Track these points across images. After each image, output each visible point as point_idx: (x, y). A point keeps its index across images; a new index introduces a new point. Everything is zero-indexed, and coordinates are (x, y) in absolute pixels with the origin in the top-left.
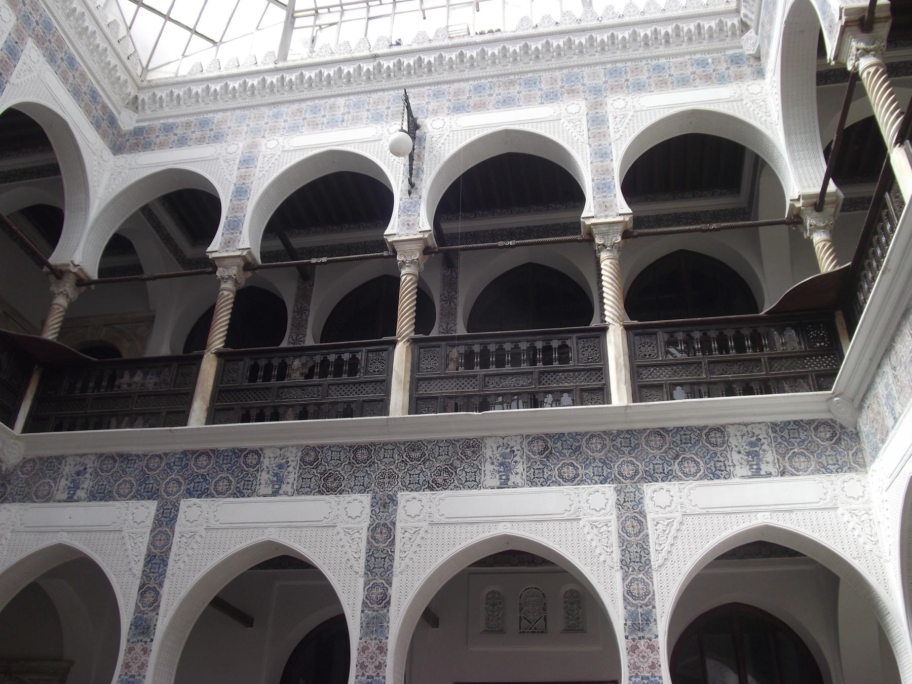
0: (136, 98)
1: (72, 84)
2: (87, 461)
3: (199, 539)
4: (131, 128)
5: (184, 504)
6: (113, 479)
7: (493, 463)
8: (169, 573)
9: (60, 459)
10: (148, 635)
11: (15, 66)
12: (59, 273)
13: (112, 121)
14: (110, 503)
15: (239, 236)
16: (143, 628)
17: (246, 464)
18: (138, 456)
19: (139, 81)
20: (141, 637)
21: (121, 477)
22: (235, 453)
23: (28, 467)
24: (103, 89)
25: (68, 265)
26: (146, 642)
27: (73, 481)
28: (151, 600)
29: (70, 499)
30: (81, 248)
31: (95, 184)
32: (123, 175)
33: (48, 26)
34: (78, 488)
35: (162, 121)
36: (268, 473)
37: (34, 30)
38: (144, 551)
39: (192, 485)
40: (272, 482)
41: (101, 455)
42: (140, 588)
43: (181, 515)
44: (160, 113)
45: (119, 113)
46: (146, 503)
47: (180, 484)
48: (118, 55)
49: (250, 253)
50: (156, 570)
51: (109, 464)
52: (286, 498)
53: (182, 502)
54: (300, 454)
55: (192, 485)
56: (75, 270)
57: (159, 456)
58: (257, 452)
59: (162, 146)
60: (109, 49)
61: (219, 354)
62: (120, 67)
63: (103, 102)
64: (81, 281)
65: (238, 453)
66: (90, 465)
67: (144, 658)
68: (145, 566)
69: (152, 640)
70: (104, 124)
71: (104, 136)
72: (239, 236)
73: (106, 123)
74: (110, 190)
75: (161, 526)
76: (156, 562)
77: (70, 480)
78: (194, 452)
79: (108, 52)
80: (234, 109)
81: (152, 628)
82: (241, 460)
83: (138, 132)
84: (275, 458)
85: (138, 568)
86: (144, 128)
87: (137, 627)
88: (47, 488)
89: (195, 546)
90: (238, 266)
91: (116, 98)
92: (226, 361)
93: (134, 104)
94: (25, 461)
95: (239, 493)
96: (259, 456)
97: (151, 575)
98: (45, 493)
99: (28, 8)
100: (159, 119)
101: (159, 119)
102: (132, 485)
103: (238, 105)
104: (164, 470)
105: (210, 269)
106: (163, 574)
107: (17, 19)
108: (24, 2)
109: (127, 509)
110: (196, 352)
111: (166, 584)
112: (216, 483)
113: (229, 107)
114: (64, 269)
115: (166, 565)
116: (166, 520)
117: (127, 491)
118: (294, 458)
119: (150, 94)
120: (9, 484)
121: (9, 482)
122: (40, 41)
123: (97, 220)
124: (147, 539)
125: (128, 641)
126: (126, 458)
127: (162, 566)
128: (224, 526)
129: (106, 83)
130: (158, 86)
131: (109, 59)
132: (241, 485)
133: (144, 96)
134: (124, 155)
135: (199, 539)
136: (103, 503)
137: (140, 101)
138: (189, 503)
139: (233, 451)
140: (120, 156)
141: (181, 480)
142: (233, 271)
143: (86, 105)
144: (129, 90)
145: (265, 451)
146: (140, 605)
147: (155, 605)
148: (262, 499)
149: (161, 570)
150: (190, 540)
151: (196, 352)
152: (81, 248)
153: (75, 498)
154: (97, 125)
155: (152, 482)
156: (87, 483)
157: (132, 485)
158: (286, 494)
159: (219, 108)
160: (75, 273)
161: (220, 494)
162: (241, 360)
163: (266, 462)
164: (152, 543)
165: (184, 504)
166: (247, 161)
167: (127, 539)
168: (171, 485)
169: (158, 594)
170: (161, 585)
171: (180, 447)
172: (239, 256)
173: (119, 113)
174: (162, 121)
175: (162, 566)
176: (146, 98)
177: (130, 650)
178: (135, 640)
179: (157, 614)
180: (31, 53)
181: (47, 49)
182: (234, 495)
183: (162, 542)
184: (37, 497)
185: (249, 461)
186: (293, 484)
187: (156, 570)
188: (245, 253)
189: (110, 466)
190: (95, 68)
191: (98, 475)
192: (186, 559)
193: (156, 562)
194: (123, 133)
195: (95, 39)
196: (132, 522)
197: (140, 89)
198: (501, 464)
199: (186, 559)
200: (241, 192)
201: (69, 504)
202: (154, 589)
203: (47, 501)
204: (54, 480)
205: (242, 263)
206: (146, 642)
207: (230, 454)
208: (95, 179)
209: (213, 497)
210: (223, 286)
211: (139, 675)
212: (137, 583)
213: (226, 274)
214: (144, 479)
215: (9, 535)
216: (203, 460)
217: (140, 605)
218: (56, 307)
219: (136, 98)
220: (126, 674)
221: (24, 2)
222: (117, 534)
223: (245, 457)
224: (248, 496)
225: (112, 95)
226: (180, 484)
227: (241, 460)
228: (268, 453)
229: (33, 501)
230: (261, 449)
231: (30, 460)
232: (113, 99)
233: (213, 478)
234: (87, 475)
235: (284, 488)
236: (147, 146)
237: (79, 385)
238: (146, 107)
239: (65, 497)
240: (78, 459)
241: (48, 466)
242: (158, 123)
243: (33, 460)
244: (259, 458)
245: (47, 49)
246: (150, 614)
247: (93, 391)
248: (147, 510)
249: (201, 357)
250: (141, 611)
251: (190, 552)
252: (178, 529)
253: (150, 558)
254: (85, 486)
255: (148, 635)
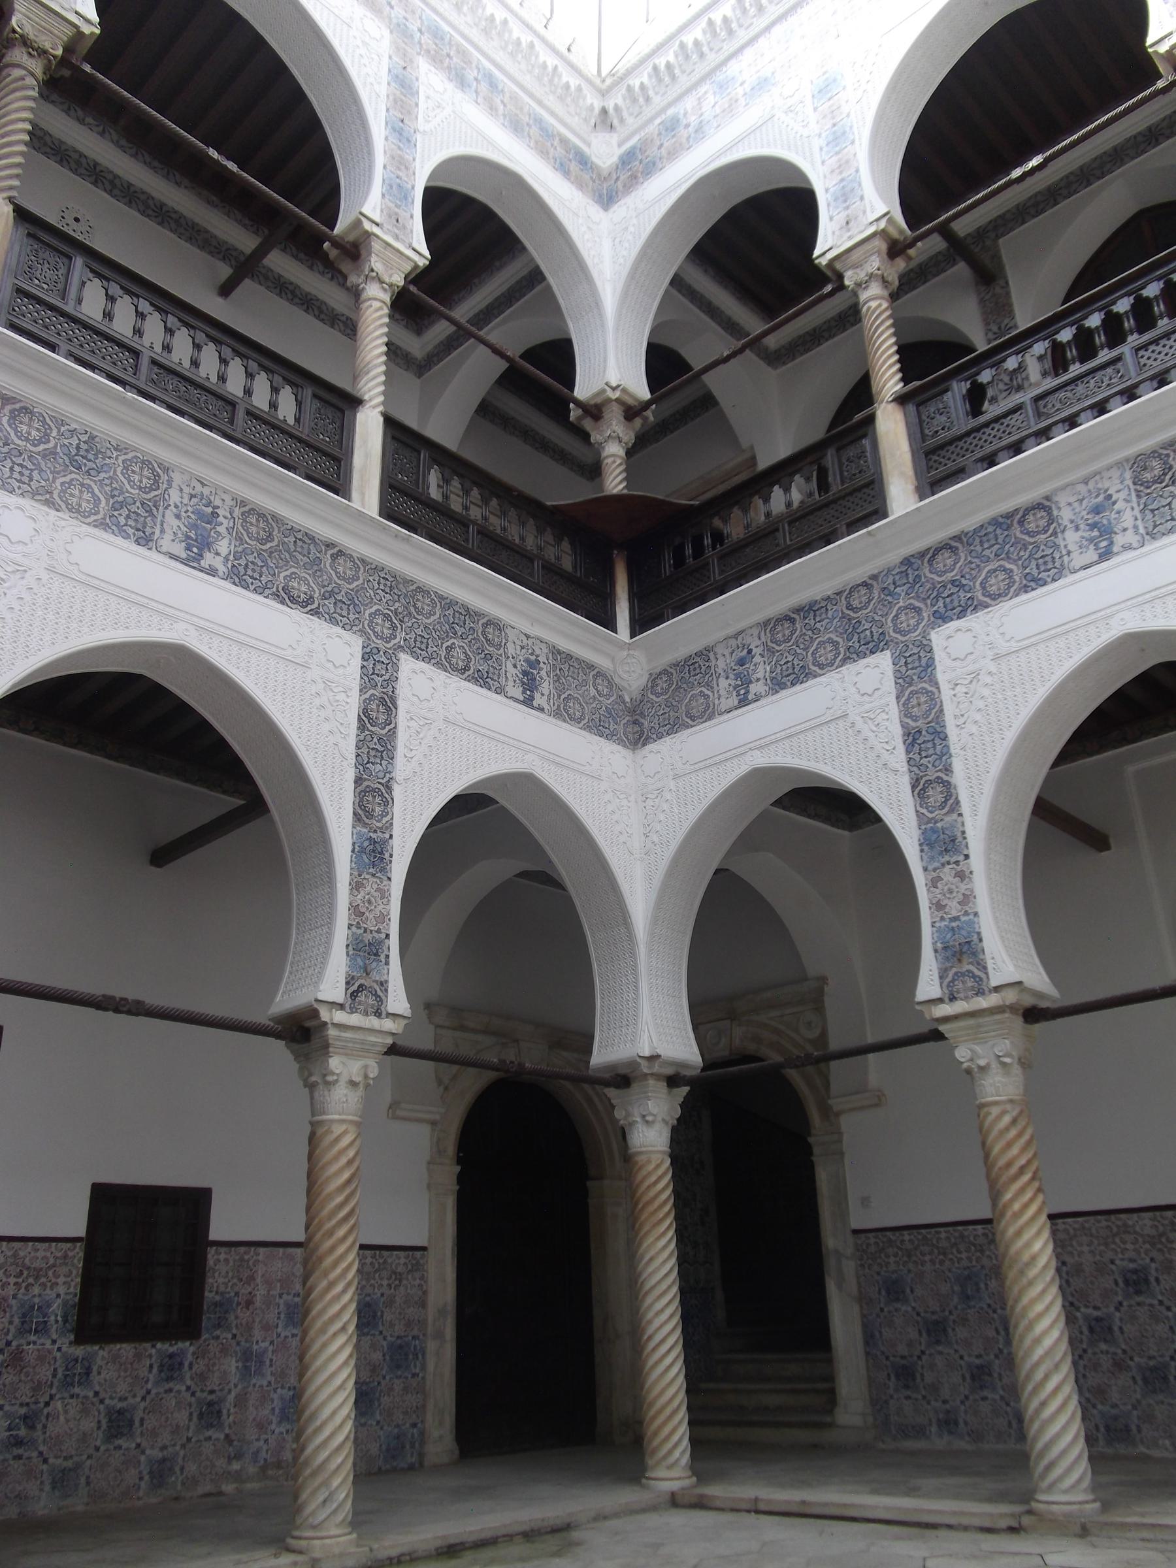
0: (604, 111)
1: (504, 116)
2: (748, 640)
3: (989, 680)
4: (615, 159)
5: (939, 638)
6: (798, 648)
7: (1077, 529)
8: (954, 749)
9: (705, 653)
10: (957, 851)
11: (417, 105)
12: (595, 411)
13: (583, 161)
14: (810, 682)
15: (856, 208)
16: (944, 843)
17: (1028, 533)
18: (828, 598)
19: (598, 81)
20: (947, 858)
21: (812, 640)
22: (1000, 525)
23: (662, 684)
24: (552, 113)
25: (603, 391)
26: (957, 863)
27: (737, 676)
28: (940, 798)
29: (744, 702)
30: (612, 364)
31: (596, 260)
32: (632, 229)
33: (437, 34)
34: (751, 682)
35: (658, 121)
36: (1077, 529)
37: (420, 43)
38: (898, 731)
39: (941, 604)
40: (1091, 540)
41: (766, 623)
42: (913, 787)
43: (939, 655)
44: (649, 112)
45: (589, 145)
46: (871, 660)
47: (918, 610)
48: (553, 49)
49: (891, 221)
50: (931, 752)
51: (785, 629)
52: (1130, 554)
53: (933, 635)
54: (1128, 475)
55: (941, 604)
56: (617, 394)
57: (865, 584)
58: (1043, 506)
59: (673, 155)
60: (537, 42)
61: (901, 400)
62: (562, 68)
63: (560, 135)
64: (631, 412)
65: (1003, 522)
66: (754, 643)
67: (963, 887)
68: (908, 752)
69: (967, 857)
70: (574, 167)
71: (580, 185)
72: (856, 208)
73: (574, 164)
74: (621, 260)
75: (910, 684)
76: (926, 741)
77: (732, 676)
78: (922, 555)
79: (537, 48)
80: (768, 29)
81: (960, 839)
82: (1017, 531)
83: (627, 159)
84: (1081, 501)
85: (899, 759)
86: (634, 147)
87: (931, 845)
88: (702, 700)
89: (986, 692)
90: (879, 252)
91: (575, 121)
92: (918, 405)
93: (605, 120)
94: (654, 679)
95: (1032, 583)
96: (1048, 510)
97: (924, 761)
98: (701, 709)
99: (398, 12)
100: (651, 120)
101: (651, 120)
102: (835, 644)
103: (773, 18)
104: (880, 601)
105: (829, 288)
106: (946, 753)
107: (391, 32)
108: (389, 4)
109: (842, 680)
110: (858, 417)
111: (957, 765)
112: (983, 585)
113: (757, 30)
114: (598, 400)
115: (945, 738)
116: (916, 672)
117: (830, 656)
118: (1120, 487)
119: (624, 91)
120: (644, 717)
121: (642, 714)
122: (437, 59)
123: (619, 315)
124: (894, 710)
125: (925, 869)
126: (809, 610)
127: (937, 741)
128: (1026, 642)
129: (551, 101)
130: (629, 73)
131: (542, 59)
132: (1032, 569)
133: (617, 99)
134: (622, 202)
135: (989, 680)
136: (798, 687)
137: (611, 111)
138: (947, 632)
139: (995, 522)
140: (615, 207)
141: (917, 604)
142: (874, 264)
143: (536, 143)
144: (589, 101)
145: (1055, 499)
146: (924, 811)
147: (950, 801)
148: (1082, 574)
149: (939, 748)
150: (972, 686)
151: (858, 417)
152: (612, 364)
153: (750, 697)
154: (563, 168)
155: (867, 626)
156: (761, 669)
157: (835, 644)
158: (1127, 548)
159: (742, 42)
160: (617, 400)
161: (996, 597)
162: (947, 390)
163: (1066, 515)
164: (906, 712)
165: (939, 638)
166: (826, 89)
167: (859, 723)
168: (903, 618)
169: (947, 785)
170: (948, 770)
171: (894, 556)
172: (874, 235)
173: (589, 145)
174: (658, 121)
175: (937, 741)
176: (620, 101)
177: (934, 883)
178: (936, 864)
179: (960, 815)
180: (430, 80)
181: (449, 68)
182: (1026, 589)
183: (924, 707)
184: (693, 718)
185: (1031, 527)
186: (1136, 527)
187: (931, 752)
188: (883, 224)
189: (787, 632)
190: (527, 80)
191: (772, 652)
192: (978, 717)
193: (926, 741)
194: (605, 173)
195: (510, 32)
196: (858, 697)
197: (603, 94)
198: (1093, 526)
199: (978, 717)
200: (838, 138)
201: (744, 709)
202: (939, 780)
203: (710, 718)
204: (708, 685)
205: (884, 247)
206: (957, 863)
207: (991, 529)
208: (592, 253)
209: (987, 607)
210: (863, 296)
211: (966, 913)
212: (905, 782)
213: (862, 275)
214: (852, 628)
215: (672, 785)
216: (945, 559)
217: (924, 811)
218: (610, 460)
219: (604, 111)
220: (942, 919)
221: (389, 4)
222: (841, 723)
223: (1021, 522)
224: (1054, 580)
225: (569, 120)
226: (918, 610)
227: (1017, 531)
228: (1062, 499)
229: (688, 727)
230: (1048, 498)
231: (660, 673)
232: (572, 124)
233: (974, 579)
234: (757, 659)
235: (1119, 540)
236: (650, 168)
237: (689, 551)
238: (625, 114)
239: (736, 702)
240: (733, 642)
241: (694, 668)
242: (652, 128)
243: (664, 672)
244: (1050, 514)
245: (449, 68)
246: (948, 819)
247: (714, 548)
248: (877, 671)
249: (871, 419)
250: (929, 820)
251: (981, 704)
252: (941, 677)
253: (912, 738)
254: (760, 675)
255: (957, 851)
